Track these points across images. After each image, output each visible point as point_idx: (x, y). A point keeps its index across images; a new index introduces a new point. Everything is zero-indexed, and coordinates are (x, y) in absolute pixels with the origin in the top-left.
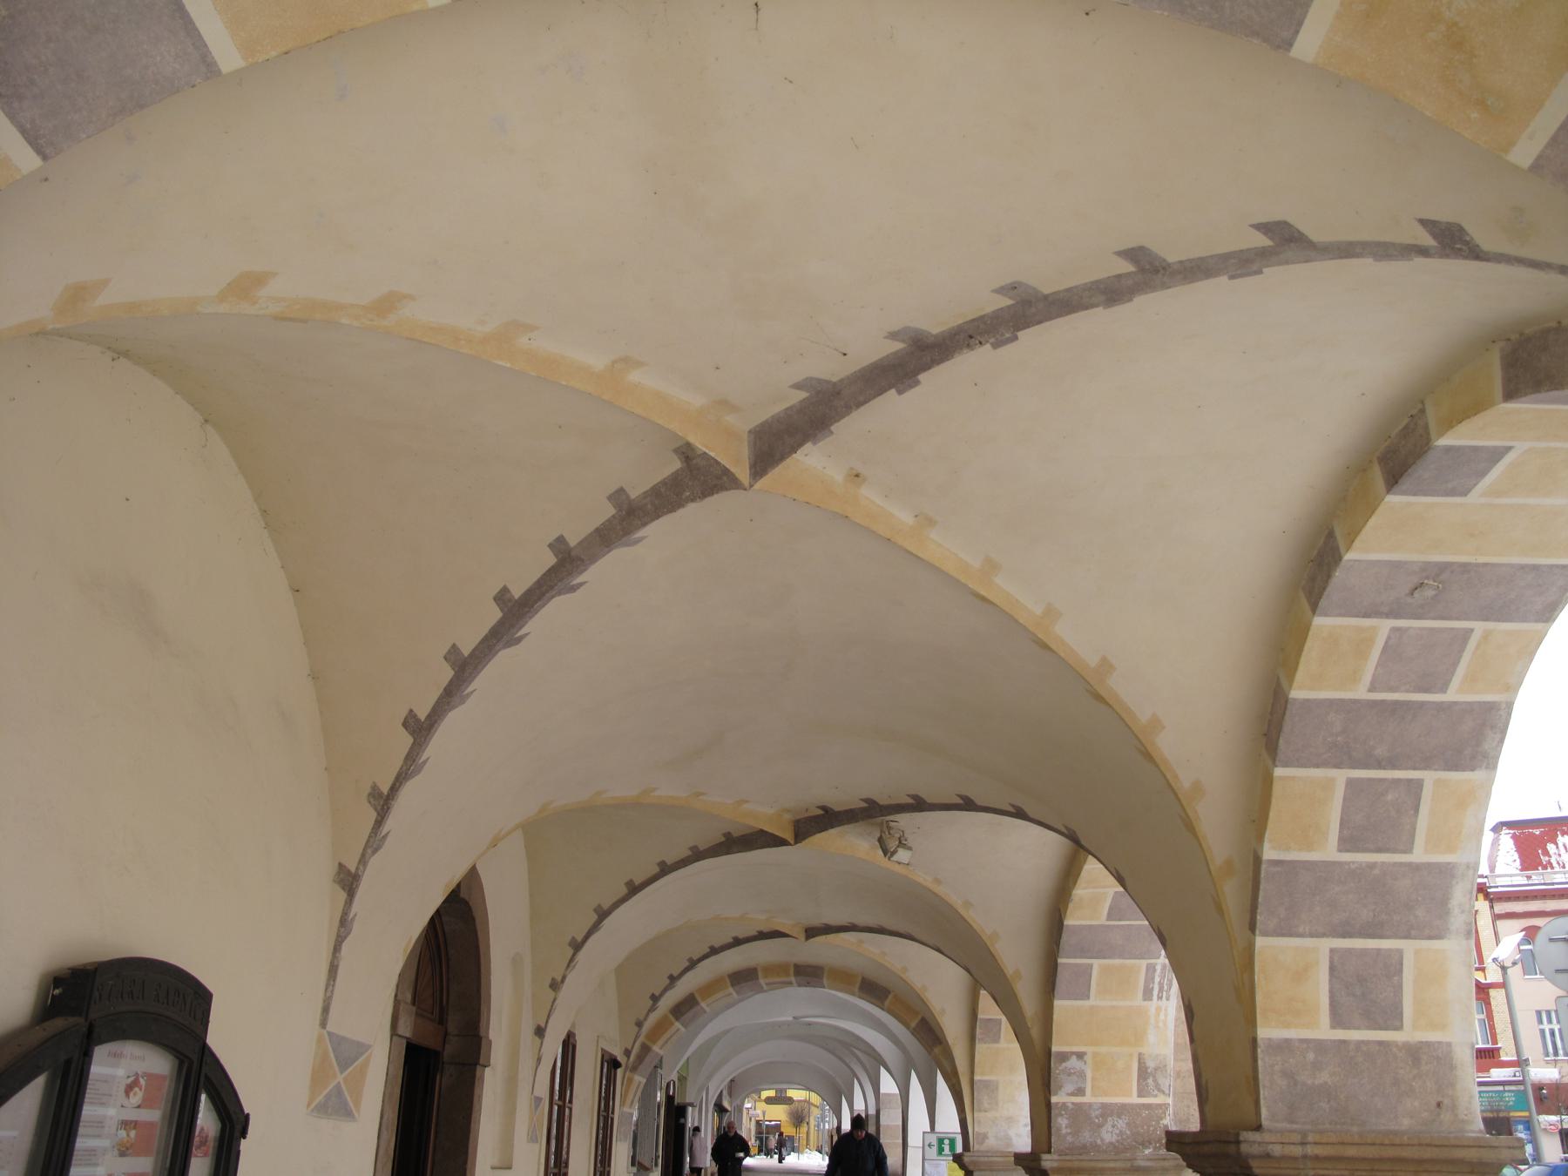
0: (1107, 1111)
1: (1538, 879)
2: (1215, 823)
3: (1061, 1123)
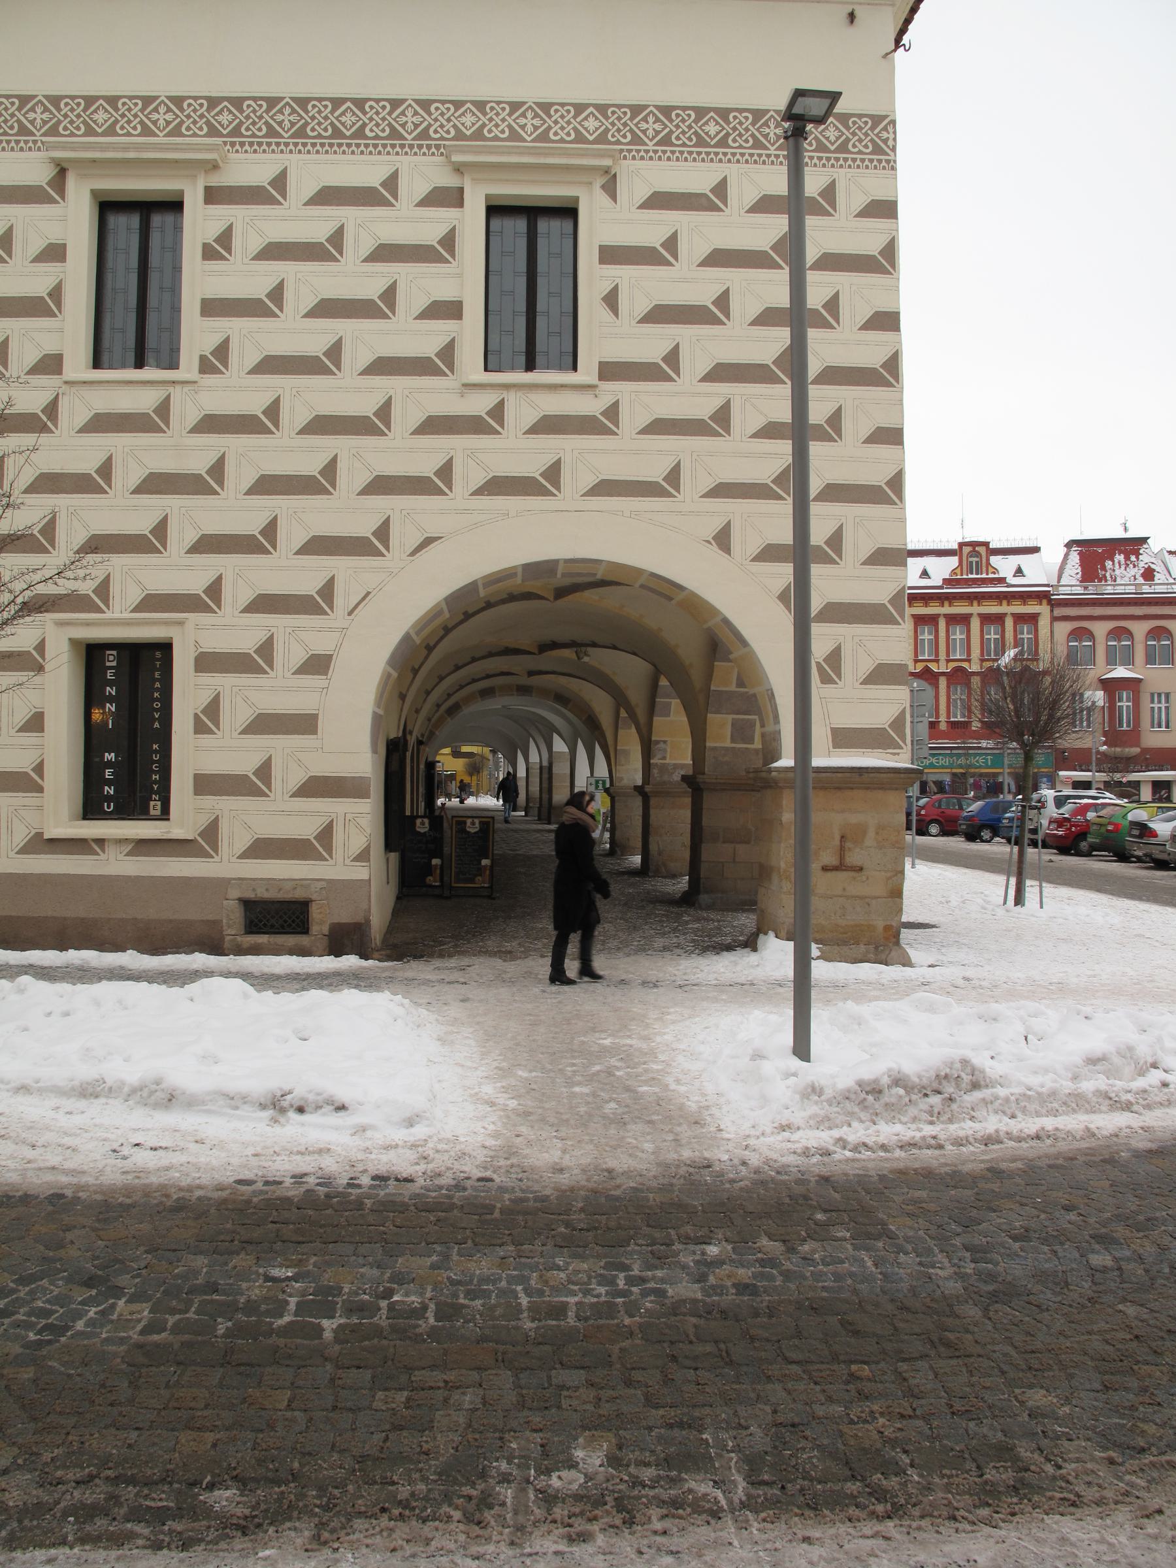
0: (676, 767)
1: (1092, 591)
2: (696, 676)
3: (655, 771)
